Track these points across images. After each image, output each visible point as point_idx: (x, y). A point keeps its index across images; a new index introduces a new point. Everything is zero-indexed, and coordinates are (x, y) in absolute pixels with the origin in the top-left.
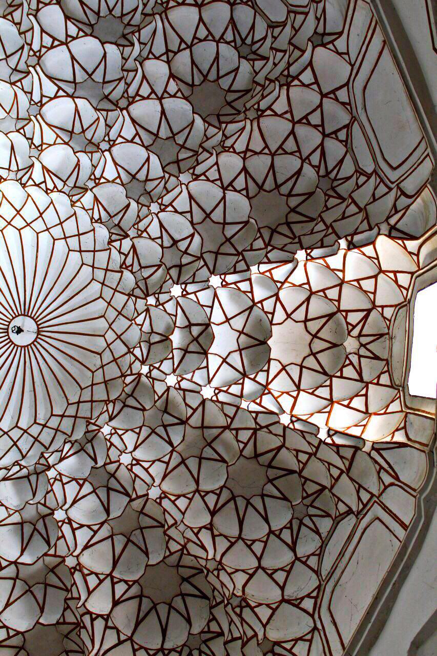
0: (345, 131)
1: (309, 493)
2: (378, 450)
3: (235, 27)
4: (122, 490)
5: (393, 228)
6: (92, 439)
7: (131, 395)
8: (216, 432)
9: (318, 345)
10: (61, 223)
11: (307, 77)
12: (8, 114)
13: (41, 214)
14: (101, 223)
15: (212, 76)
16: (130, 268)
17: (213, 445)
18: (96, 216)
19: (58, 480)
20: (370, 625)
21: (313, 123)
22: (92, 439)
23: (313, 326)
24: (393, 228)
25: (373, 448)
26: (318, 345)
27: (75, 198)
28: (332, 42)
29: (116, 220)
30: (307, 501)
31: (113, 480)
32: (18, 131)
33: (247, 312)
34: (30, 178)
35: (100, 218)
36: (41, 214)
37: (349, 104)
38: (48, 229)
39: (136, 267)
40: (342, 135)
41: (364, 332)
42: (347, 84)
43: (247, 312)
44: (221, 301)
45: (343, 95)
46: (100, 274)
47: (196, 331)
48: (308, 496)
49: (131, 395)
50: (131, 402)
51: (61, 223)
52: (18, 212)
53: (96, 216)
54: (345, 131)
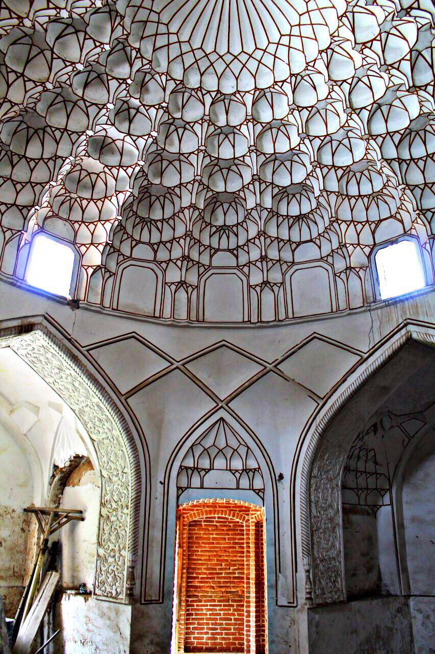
0: (156, 249)
1: (13, 157)
2: (20, 235)
3: (235, 234)
4: (63, 34)
5: (101, 268)
6: (110, 14)
7: (124, 49)
8: (69, 109)
9: (84, 173)
10: (260, 62)
11: (179, 263)
12: (326, 109)
13: (275, 57)
14: (232, 94)
15: (233, 204)
16: (196, 90)
17: (63, 103)
18: (238, 95)
19: (91, 5)
20: (20, 607)
21: (168, 243)
22: (110, 14)
23: (94, 177)
24: (101, 268)
25: (22, 233)
26: (84, 173)
27: (257, 92)
28: (177, 286)
29: (227, 101)
30: (9, 153)
31: (73, 30)
32: (312, 107)
33: (121, 151)
34: (291, 83)
35: (235, 96)
36: (275, 57)
37: (160, 264)
38: (265, 51)
39: (193, 93)
40: (156, 247)
41: (76, 202)
42: (165, 271)
43: (121, 151)
44: (134, 150)
45: (164, 265)
46: (213, 57)
47: (133, 112)
48: (12, 155)
49: (124, 49)
50: (120, 46)
51: (260, 62)
52: (289, 47)
53: (238, 95)
54: (156, 249)
